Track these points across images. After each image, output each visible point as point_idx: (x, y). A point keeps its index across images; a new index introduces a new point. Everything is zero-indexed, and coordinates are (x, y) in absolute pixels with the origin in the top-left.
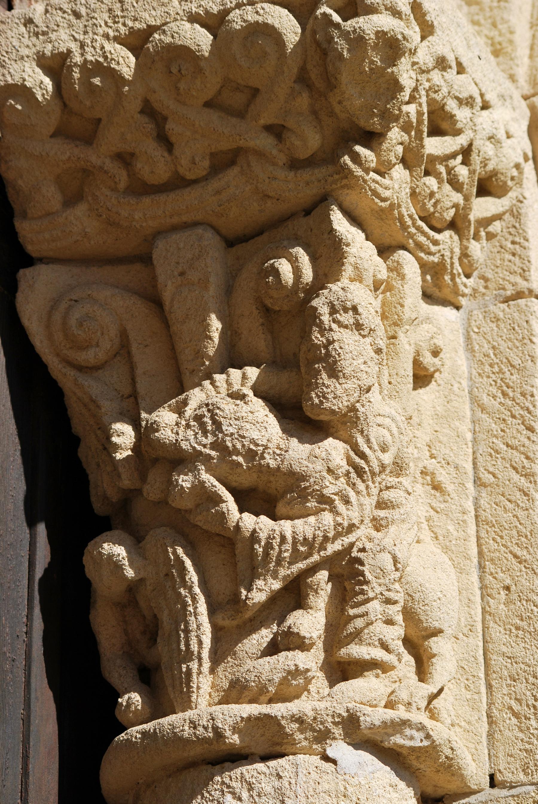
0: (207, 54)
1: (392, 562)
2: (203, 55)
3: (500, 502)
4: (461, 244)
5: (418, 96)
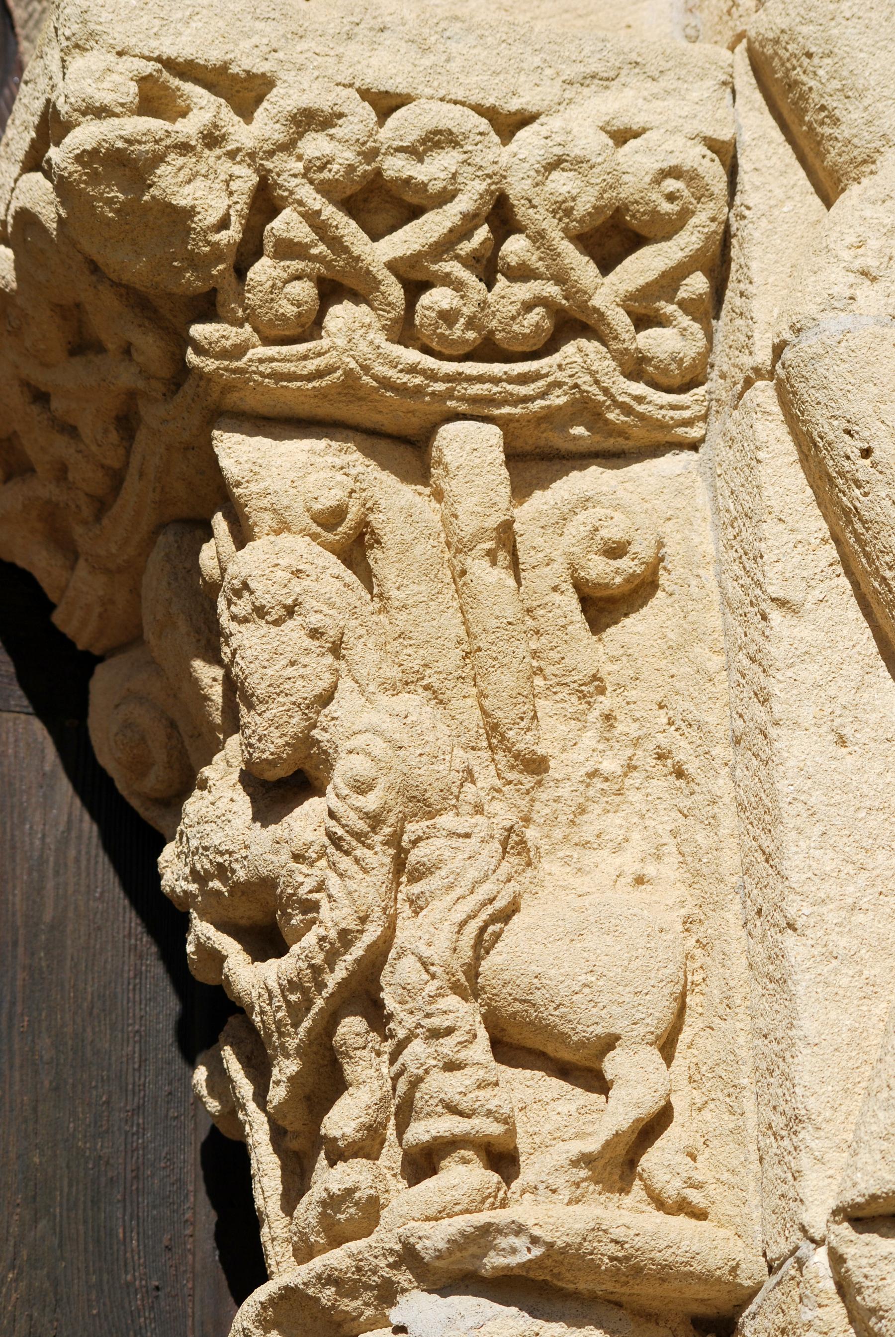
0: (14, 285)
1: (422, 968)
2: (12, 290)
4: (610, 352)
5: (286, 194)
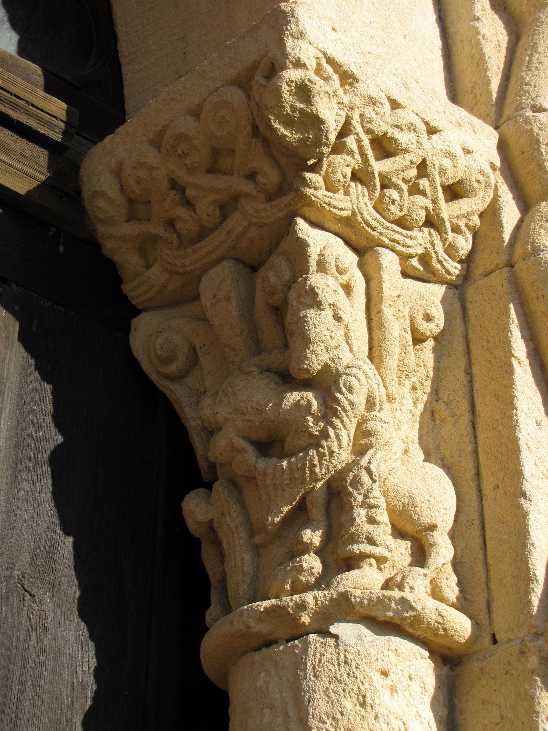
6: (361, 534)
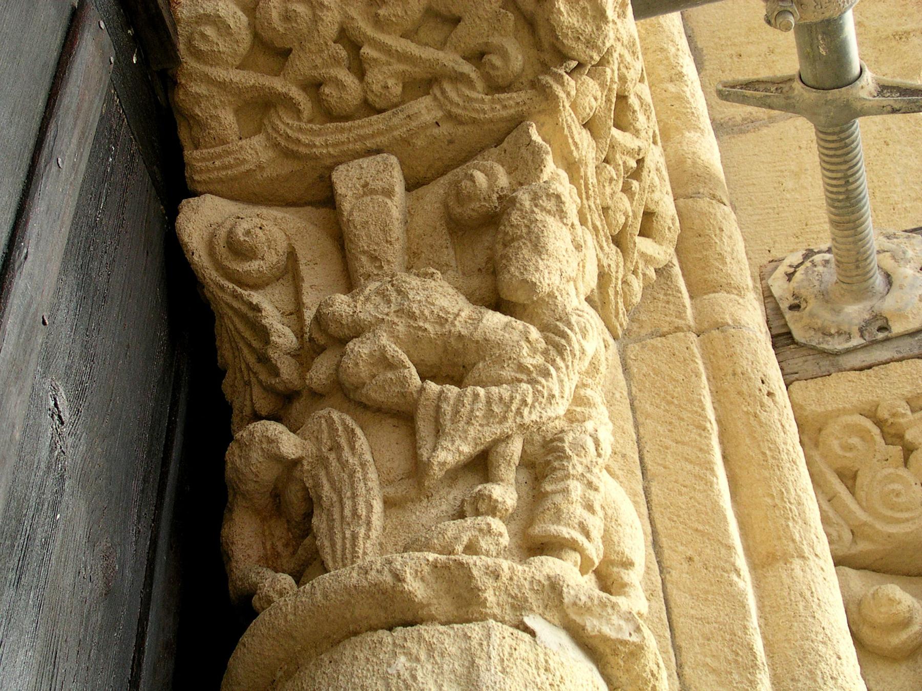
3: (673, 487)
6: (572, 516)
